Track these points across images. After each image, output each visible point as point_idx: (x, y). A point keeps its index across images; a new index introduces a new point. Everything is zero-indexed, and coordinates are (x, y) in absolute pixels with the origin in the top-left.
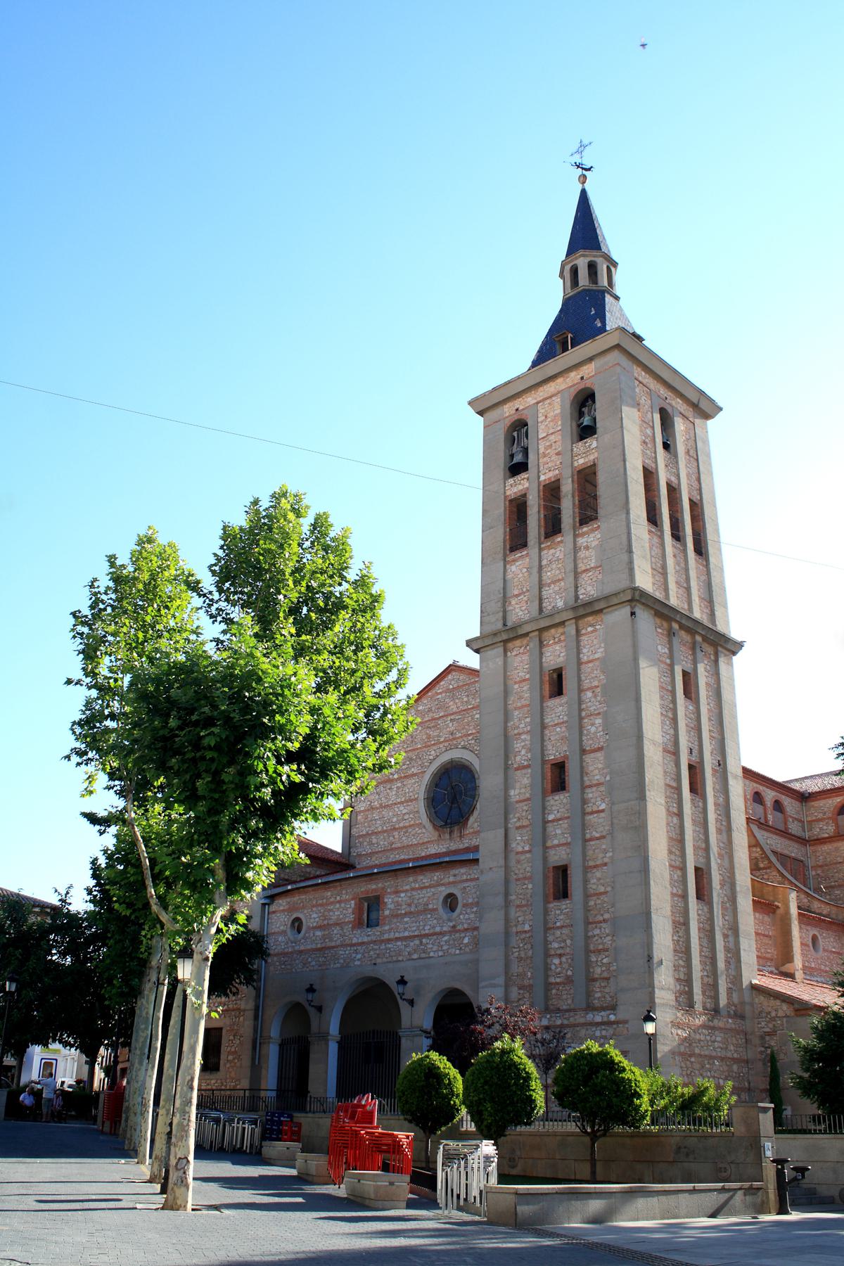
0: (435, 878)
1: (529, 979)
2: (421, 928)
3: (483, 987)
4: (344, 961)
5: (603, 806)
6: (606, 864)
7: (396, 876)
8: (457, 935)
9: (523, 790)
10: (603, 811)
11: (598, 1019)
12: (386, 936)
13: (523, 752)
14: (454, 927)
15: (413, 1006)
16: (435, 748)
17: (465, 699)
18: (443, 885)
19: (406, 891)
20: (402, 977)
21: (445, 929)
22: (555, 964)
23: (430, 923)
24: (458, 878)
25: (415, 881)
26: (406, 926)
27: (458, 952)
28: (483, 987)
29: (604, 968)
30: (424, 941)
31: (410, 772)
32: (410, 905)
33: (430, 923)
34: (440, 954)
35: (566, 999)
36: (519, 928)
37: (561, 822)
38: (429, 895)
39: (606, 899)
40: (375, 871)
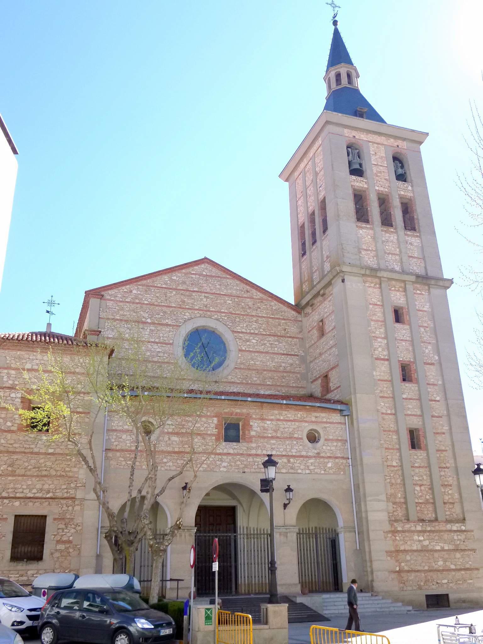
0: (299, 416)
1: (400, 498)
2: (288, 450)
3: (370, 501)
4: (208, 466)
5: (438, 398)
6: (444, 433)
7: (262, 407)
8: (322, 460)
9: (382, 374)
10: (438, 401)
11: (455, 528)
12: (253, 452)
13: (380, 349)
14: (318, 453)
15: (285, 509)
16: (190, 311)
17: (218, 287)
18: (306, 422)
19: (272, 420)
20: (289, 486)
21: (310, 454)
22: (417, 490)
23: (297, 447)
24: (319, 420)
25: (280, 414)
26: (273, 447)
27: (323, 472)
28: (370, 501)
29: (450, 497)
30: (292, 460)
31: (165, 322)
32: (276, 431)
33: (297, 447)
34: (308, 472)
35: (428, 514)
36: (389, 463)
37: (411, 401)
38: (293, 427)
39: (446, 454)
40: (249, 399)
